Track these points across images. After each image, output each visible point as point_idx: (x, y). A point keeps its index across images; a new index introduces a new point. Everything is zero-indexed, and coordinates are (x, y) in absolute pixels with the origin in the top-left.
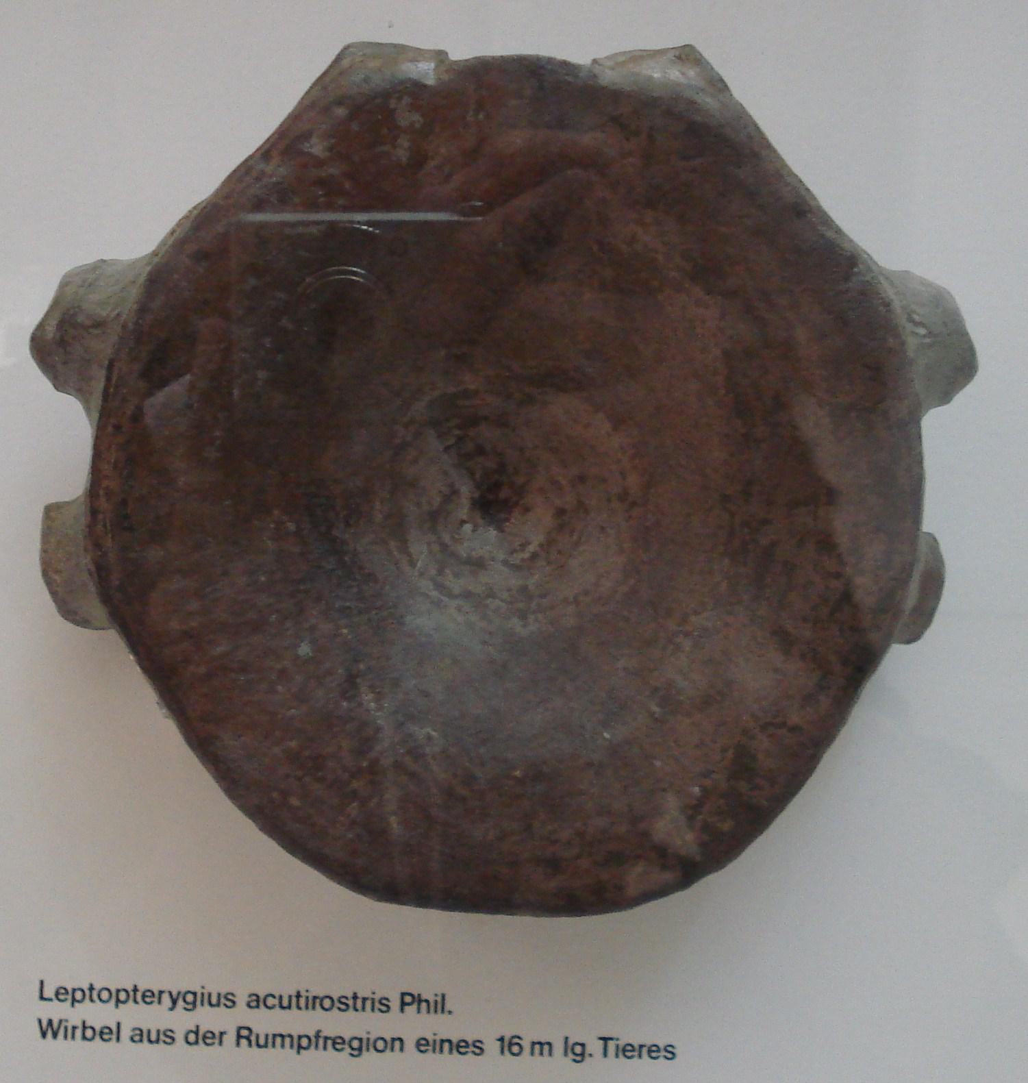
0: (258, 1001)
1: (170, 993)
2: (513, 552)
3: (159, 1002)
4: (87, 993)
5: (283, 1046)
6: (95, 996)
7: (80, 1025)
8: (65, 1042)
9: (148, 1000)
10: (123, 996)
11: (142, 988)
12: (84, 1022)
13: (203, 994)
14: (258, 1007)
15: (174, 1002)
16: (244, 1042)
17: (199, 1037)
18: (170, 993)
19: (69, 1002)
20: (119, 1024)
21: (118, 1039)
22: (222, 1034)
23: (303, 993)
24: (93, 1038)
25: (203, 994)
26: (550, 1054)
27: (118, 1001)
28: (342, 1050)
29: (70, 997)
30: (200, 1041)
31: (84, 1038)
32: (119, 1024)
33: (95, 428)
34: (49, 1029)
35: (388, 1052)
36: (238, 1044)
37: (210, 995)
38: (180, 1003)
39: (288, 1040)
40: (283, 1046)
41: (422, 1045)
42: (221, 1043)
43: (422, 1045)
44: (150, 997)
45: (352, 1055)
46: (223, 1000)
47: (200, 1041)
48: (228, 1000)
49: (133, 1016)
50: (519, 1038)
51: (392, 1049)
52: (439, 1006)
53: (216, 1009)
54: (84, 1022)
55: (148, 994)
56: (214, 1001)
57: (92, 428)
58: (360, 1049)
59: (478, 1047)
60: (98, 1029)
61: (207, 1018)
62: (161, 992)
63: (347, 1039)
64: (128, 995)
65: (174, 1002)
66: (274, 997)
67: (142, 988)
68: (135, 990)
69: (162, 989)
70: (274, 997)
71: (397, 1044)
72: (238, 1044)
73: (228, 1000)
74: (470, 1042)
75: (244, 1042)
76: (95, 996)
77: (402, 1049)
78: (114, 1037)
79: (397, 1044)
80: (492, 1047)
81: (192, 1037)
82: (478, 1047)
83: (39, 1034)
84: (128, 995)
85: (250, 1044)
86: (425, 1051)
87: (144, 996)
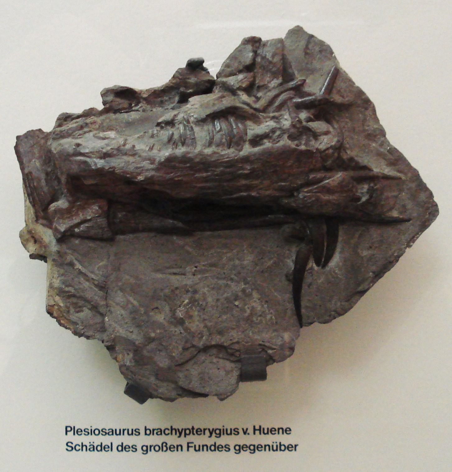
1: (209, 430)
2: (396, 197)
3: (204, 434)
4: (191, 431)
6: (195, 432)
8: (207, 452)
9: (199, 433)
11: (196, 427)
12: (82, 443)
13: (223, 430)
14: (161, 434)
15: (211, 434)
16: (257, 432)
17: (123, 448)
18: (209, 430)
20: (112, 444)
21: (112, 450)
22: (296, 446)
24: (285, 450)
25: (223, 430)
26: (182, 450)
28: (246, 450)
30: (124, 450)
32: (112, 444)
33: (113, 88)
34: (70, 447)
36: (254, 433)
37: (227, 430)
38: (214, 434)
42: (295, 450)
44: (80, 432)
45: (251, 453)
46: (233, 432)
47: (124, 450)
48: (136, 432)
49: (116, 440)
50: (67, 450)
53: (131, 436)
54: (82, 443)
55: (199, 430)
56: (229, 432)
57: (113, 87)
58: (220, 434)
59: (227, 448)
60: (286, 446)
61: (128, 440)
63: (248, 445)
65: (211, 434)
66: (168, 429)
67: (196, 427)
68: (193, 428)
69: (205, 428)
71: (180, 448)
72: (254, 433)
73: (136, 432)
74: (224, 446)
76: (195, 432)
77: (182, 450)
78: (110, 449)
79: (180, 448)
80: (241, 432)
81: (120, 448)
82: (227, 448)
86: (292, 450)
87: (197, 432)
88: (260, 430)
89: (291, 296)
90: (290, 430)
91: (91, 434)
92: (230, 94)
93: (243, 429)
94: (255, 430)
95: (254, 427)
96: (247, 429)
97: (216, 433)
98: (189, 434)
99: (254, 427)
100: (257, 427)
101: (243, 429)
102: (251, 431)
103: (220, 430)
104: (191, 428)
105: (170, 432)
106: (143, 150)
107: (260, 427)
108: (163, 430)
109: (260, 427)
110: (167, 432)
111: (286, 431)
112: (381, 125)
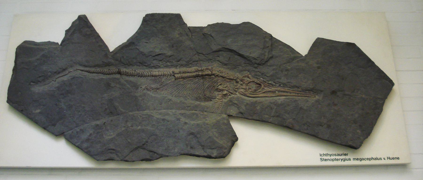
0: (338, 155)
1: (341, 159)
3: (339, 160)
5: (355, 160)
6: (336, 160)
7: (327, 154)
10: (334, 160)
19: (369, 160)
23: (327, 154)
27: (333, 161)
29: (369, 159)
31: (361, 159)
35: (372, 160)
36: (388, 159)
39: (355, 159)
40: (355, 160)
41: (381, 159)
43: (381, 159)
51: (372, 160)
52: (398, 158)
58: (345, 160)
62: (339, 159)
64: (334, 160)
66: (322, 154)
70: (322, 154)
72: (388, 159)
75: (388, 159)
76: (336, 160)
83: (320, 155)
84: (334, 160)
85: (389, 159)
88: (389, 158)
89: (210, 73)
90: (399, 158)
91: (324, 161)
92: (174, 69)
93: (384, 158)
94: (388, 158)
95: (387, 157)
96: (385, 158)
97: (343, 160)
98: (334, 161)
99: (387, 157)
100: (388, 157)
101: (384, 158)
102: (386, 158)
103: (344, 159)
104: (335, 159)
105: (323, 155)
106: (207, 101)
107: (389, 157)
108: (364, 159)
109: (389, 157)
110: (365, 159)
111: (357, 159)
112: (368, 137)
